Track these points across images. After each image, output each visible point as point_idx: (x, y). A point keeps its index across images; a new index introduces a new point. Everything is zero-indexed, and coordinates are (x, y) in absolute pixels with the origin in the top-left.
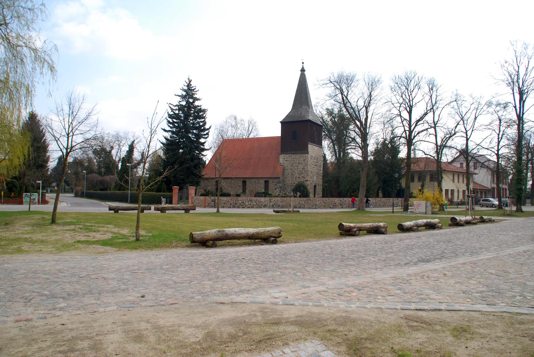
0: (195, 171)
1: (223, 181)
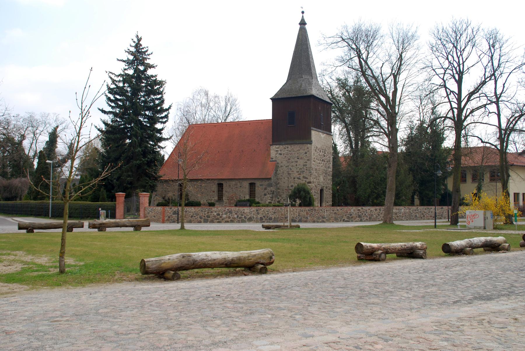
0: (149, 171)
1: (189, 184)
